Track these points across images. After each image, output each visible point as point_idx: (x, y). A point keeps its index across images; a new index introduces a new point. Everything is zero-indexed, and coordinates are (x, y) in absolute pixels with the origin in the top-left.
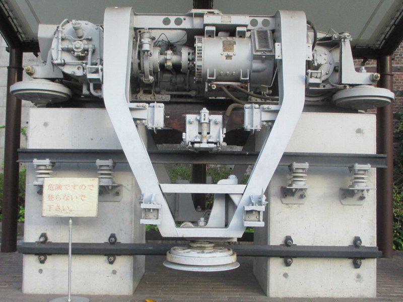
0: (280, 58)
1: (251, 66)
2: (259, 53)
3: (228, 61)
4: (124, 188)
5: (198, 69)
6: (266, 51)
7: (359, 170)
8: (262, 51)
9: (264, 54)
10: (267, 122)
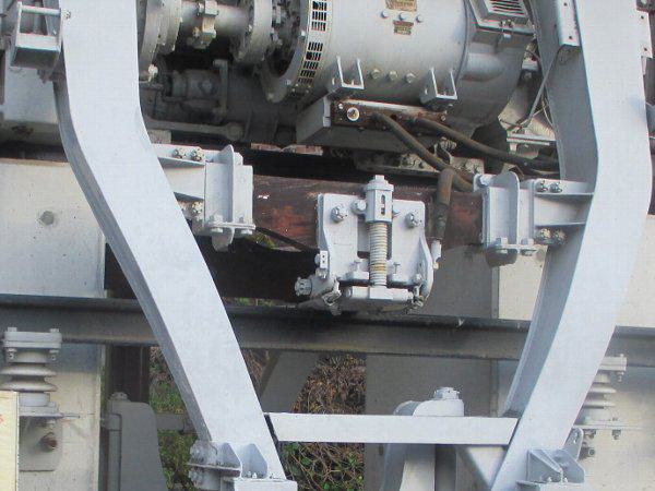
0: (574, 43)
1: (463, 59)
2: (494, 24)
3: (401, 38)
4: (66, 428)
5: (309, 56)
6: (513, 19)
7: (20, 351)
8: (501, 18)
9: (507, 28)
10: (553, 229)
